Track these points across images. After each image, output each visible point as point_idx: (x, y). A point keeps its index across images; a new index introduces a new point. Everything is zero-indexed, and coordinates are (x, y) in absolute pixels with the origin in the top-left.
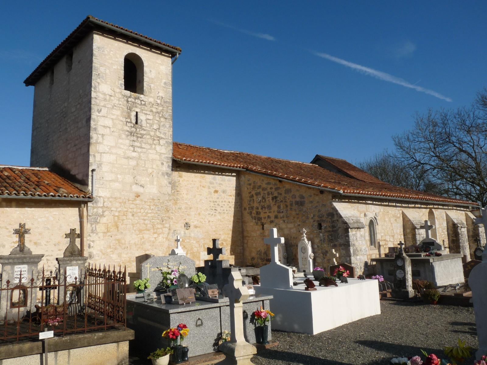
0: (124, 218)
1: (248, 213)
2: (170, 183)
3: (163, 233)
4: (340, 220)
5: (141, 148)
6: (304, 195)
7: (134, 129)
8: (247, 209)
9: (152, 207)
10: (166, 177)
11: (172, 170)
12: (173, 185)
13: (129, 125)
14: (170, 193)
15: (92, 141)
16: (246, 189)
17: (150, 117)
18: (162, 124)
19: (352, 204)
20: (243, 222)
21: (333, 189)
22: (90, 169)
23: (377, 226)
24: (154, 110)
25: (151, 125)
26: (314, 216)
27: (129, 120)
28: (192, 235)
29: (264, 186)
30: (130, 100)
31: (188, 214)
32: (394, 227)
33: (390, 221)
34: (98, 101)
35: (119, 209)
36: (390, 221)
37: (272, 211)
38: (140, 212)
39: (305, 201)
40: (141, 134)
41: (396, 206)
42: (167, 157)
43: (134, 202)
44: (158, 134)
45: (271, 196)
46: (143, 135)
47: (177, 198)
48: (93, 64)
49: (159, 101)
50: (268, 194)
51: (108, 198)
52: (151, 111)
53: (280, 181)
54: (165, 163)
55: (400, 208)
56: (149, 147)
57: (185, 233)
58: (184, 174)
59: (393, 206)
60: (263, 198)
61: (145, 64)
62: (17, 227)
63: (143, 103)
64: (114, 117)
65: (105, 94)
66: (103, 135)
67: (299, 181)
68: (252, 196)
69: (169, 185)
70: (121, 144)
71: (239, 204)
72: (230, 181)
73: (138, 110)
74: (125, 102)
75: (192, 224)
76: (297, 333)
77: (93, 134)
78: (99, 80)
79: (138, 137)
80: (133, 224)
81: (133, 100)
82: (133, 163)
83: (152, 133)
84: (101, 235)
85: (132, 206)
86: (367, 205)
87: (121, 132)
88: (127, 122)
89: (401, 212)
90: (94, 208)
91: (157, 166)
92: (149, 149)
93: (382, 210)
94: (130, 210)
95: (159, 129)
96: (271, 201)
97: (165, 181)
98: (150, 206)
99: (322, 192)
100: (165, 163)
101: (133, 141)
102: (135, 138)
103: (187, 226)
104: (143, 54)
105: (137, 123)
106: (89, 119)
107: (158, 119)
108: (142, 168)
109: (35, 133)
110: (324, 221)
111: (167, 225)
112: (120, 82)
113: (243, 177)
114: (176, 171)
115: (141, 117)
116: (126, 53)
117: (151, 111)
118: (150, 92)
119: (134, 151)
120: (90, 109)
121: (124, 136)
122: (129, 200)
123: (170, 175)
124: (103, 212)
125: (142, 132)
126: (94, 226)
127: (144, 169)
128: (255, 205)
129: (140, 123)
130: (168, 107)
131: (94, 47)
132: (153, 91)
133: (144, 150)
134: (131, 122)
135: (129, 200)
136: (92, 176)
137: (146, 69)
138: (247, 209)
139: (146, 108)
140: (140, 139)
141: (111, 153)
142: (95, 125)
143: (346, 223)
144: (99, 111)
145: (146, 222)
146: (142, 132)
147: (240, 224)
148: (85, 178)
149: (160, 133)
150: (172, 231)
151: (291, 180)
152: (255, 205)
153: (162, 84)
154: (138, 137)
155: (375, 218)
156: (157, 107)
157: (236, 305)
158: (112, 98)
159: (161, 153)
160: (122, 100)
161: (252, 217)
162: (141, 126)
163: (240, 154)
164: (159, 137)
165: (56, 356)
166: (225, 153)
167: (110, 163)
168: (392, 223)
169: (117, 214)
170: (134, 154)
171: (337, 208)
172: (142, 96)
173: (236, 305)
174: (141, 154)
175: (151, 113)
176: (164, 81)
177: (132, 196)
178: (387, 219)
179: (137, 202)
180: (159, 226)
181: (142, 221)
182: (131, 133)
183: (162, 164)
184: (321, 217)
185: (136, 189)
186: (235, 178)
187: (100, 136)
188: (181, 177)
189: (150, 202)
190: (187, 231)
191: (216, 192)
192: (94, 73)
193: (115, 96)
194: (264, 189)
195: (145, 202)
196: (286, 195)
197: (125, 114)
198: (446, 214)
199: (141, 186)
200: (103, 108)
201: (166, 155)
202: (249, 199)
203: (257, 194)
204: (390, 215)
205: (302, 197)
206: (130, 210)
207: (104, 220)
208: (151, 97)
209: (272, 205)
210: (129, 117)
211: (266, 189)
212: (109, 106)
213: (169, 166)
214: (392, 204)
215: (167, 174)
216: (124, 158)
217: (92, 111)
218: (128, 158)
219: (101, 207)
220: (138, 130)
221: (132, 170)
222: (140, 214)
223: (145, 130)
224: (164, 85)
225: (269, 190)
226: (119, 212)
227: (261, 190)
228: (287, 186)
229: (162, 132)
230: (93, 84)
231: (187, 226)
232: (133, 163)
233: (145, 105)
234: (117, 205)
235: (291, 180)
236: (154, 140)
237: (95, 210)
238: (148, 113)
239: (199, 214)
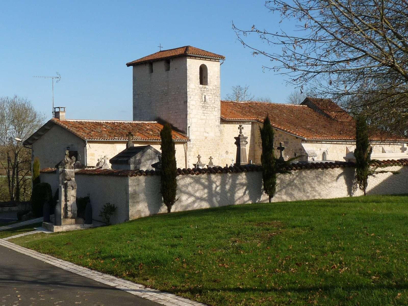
0: (201, 149)
1: (258, 146)
2: (219, 131)
3: (216, 156)
4: (304, 153)
5: (207, 113)
6: (288, 138)
7: (204, 104)
8: (257, 143)
9: (212, 143)
10: (218, 127)
11: (220, 124)
12: (221, 131)
13: (202, 102)
14: (219, 136)
15: (188, 113)
16: (257, 132)
17: (211, 97)
18: (216, 100)
19: (312, 144)
20: (255, 151)
21: (302, 137)
22: (188, 126)
23: (327, 155)
24: (212, 93)
25: (211, 101)
26: (293, 149)
27: (202, 100)
28: (229, 157)
30: (202, 89)
31: (227, 146)
32: (339, 156)
33: (337, 152)
34: (190, 93)
35: (199, 145)
36: (337, 152)
38: (207, 146)
39: (288, 142)
40: (207, 106)
41: (342, 144)
42: (218, 117)
43: (205, 141)
44: (214, 105)
46: (208, 107)
47: (223, 139)
48: (187, 74)
49: (214, 88)
51: (195, 140)
52: (211, 93)
53: (276, 130)
54: (217, 120)
55: (345, 145)
56: (210, 113)
57: (226, 156)
58: (226, 125)
59: (340, 144)
61: (208, 69)
62: (209, 157)
63: (207, 90)
65: (192, 89)
66: (192, 109)
67: (286, 131)
69: (219, 132)
70: (199, 112)
71: (252, 140)
72: (248, 127)
73: (205, 94)
74: (200, 91)
75: (229, 152)
77: (188, 110)
78: (190, 82)
79: (206, 108)
80: (204, 152)
81: (203, 89)
82: (204, 121)
84: (192, 157)
85: (204, 143)
86: (322, 144)
87: (199, 107)
88: (201, 101)
89: (345, 147)
90: (189, 144)
91: (214, 122)
92: (210, 114)
93: (332, 147)
94: (203, 145)
95: (215, 103)
97: (217, 130)
98: (211, 143)
99: (297, 138)
100: (217, 120)
101: (204, 110)
102: (204, 109)
103: (227, 152)
104: (207, 63)
105: (205, 101)
106: (186, 102)
107: (214, 97)
108: (207, 124)
109: (137, 97)
110: (297, 152)
111: (218, 152)
112: (198, 81)
113: (255, 125)
114: (222, 124)
116: (200, 65)
117: (211, 93)
118: (210, 84)
119: (204, 116)
120: (187, 97)
121: (200, 109)
122: (202, 140)
123: (220, 126)
124: (193, 146)
125: (208, 105)
126: (190, 152)
127: (209, 124)
129: (207, 101)
130: (218, 90)
131: (187, 66)
132: (212, 82)
133: (208, 115)
134: (203, 101)
135: (202, 140)
136: (189, 129)
137: (208, 71)
138: (257, 143)
139: (209, 92)
140: (206, 109)
142: (189, 105)
143: (307, 154)
144: (190, 98)
145: (210, 151)
146: (208, 105)
147: (253, 151)
148: (184, 130)
149: (215, 104)
150: (220, 155)
151: (282, 130)
153: (216, 78)
154: (206, 108)
155: (327, 151)
156: (213, 91)
157: (282, 151)
158: (195, 90)
159: (215, 115)
160: (199, 90)
161: (260, 148)
162: (207, 102)
163: (251, 103)
164: (214, 107)
167: (195, 123)
168: (338, 154)
169: (198, 147)
170: (205, 117)
171: (304, 146)
172: (207, 86)
173: (282, 151)
174: (207, 117)
175: (211, 95)
176: (216, 76)
177: (204, 138)
178: (335, 151)
179: (206, 141)
180: (215, 153)
181: (208, 150)
182: (203, 107)
183: (216, 121)
184: (296, 150)
185: (206, 135)
186: (251, 125)
187: (191, 110)
188: (224, 127)
189: (211, 141)
190: (227, 155)
192: (188, 79)
193: (196, 89)
195: (209, 141)
196: (279, 138)
197: (200, 97)
198: (383, 148)
199: (207, 133)
200: (192, 96)
201: (218, 116)
202: (258, 137)
204: (337, 149)
205: (287, 139)
206: (203, 145)
207: (193, 150)
208: (211, 86)
210: (202, 98)
212: (194, 94)
213: (219, 122)
214: (339, 143)
215: (218, 126)
216: (201, 120)
217: (188, 98)
218: (202, 119)
219: (192, 144)
220: (206, 104)
221: (203, 125)
222: (207, 147)
223: (208, 104)
224: (217, 78)
226: (199, 146)
228: (280, 133)
229: (216, 104)
230: (188, 85)
231: (227, 152)
232: (204, 121)
233: (208, 91)
234: (198, 142)
235: (282, 130)
236: (212, 109)
237: (190, 145)
238: (210, 95)
239: (233, 146)
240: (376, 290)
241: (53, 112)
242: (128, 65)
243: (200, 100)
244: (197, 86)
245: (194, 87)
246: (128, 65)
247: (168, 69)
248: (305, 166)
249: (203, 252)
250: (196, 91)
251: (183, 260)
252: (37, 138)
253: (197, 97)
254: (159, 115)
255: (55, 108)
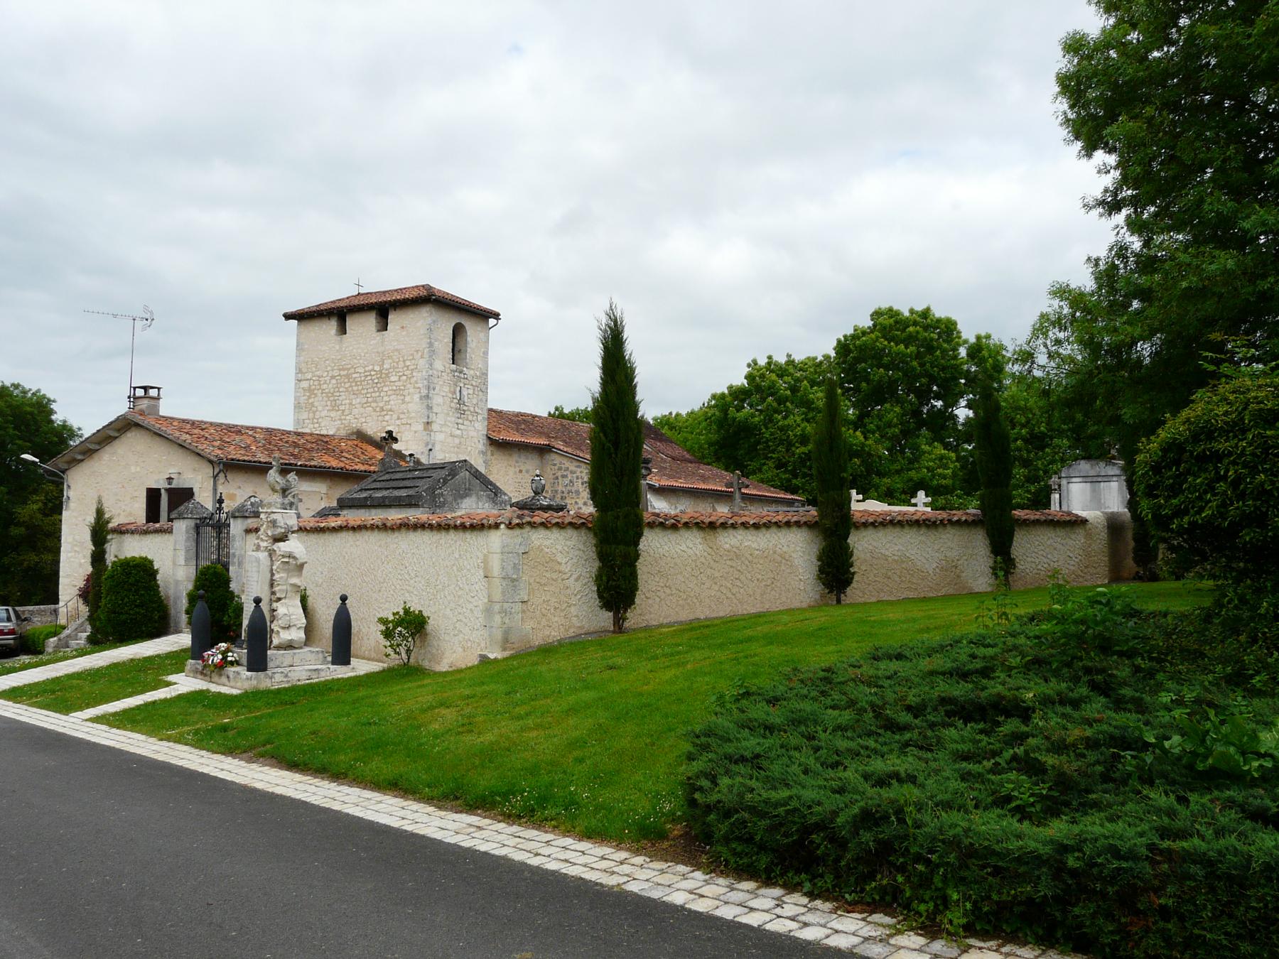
29: (574, 469)
37: (581, 496)
40: (464, 410)
45: (580, 481)
50: (577, 478)
60: (571, 481)
64: (444, 394)
65: (437, 371)
68: (557, 478)
70: (449, 421)
73: (462, 385)
76: (273, 575)
82: (457, 441)
83: (472, 409)
96: (580, 485)
115: (465, 392)
125: (465, 408)
128: (560, 488)
141: (441, 432)
152: (560, 488)
165: (99, 503)
166: (858, 912)
170: (459, 432)
191: (521, 471)
194: (572, 472)
203: (563, 476)
209: (581, 490)
210: (454, 393)
211: (575, 473)
225: (578, 474)
227: (568, 472)
232: (457, 441)
238: (469, 387)
240: (959, 719)
241: (129, 397)
242: (288, 317)
243: (450, 395)
244: (447, 366)
245: (441, 368)
246: (288, 317)
247: (384, 327)
248: (1242, 20)
249: (430, 684)
250: (446, 377)
251: (1123, 376)
252: (117, 435)
253: (446, 389)
254: (359, 425)
255: (135, 388)
